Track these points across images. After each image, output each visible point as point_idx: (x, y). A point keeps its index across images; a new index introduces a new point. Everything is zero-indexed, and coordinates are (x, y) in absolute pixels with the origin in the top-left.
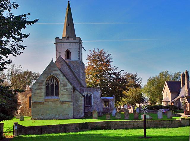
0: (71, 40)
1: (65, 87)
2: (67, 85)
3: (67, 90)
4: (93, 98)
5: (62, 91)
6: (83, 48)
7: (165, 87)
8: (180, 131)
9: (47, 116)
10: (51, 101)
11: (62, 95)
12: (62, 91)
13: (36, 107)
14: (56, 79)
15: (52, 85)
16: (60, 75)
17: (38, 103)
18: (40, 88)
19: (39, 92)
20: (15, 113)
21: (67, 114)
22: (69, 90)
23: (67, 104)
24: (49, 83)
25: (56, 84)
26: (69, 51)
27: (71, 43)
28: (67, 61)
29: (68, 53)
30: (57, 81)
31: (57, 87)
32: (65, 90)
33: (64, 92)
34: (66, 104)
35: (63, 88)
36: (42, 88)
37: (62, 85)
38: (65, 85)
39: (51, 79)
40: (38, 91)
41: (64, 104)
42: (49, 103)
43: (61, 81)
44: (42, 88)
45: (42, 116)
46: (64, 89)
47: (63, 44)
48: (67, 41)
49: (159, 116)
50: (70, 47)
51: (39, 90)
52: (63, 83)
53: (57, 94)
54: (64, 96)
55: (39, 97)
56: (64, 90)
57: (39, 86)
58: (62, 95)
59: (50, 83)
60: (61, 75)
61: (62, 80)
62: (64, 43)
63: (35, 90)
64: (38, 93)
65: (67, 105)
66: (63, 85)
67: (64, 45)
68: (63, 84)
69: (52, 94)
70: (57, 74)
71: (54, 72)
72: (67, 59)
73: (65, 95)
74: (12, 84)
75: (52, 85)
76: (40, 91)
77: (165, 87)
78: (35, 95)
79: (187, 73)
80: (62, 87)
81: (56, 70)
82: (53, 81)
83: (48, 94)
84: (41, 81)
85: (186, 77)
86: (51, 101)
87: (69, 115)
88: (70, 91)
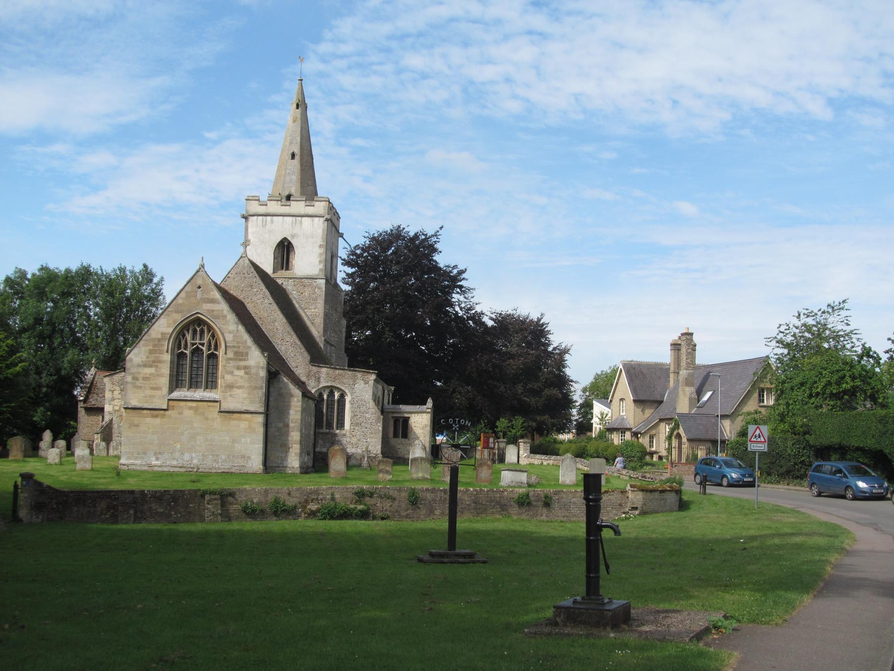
0: (298, 207)
1: (241, 360)
2: (247, 354)
3: (246, 373)
4: (348, 406)
5: (228, 371)
6: (341, 235)
7: (617, 383)
8: (752, 544)
9: (174, 459)
10: (191, 408)
11: (230, 387)
12: (232, 373)
13: (137, 426)
14: (210, 328)
15: (197, 351)
16: (226, 317)
17: (145, 412)
18: (154, 362)
19: (151, 374)
20: (35, 478)
21: (243, 457)
22: (253, 371)
23: (246, 420)
24: (186, 345)
25: (209, 350)
26: (290, 243)
27: (299, 218)
28: (281, 278)
29: (285, 250)
30: (213, 336)
31: (213, 357)
32: (241, 373)
33: (236, 378)
34: (240, 419)
35: (232, 363)
36: (160, 362)
37: (230, 354)
38: (241, 355)
39: (195, 331)
40: (148, 371)
41: (235, 419)
42: (181, 413)
43: (229, 337)
44: (160, 362)
45: (157, 459)
46: (238, 368)
47: (269, 218)
48: (285, 210)
49: (563, 476)
50: (295, 232)
51: (151, 366)
52: (233, 347)
53: (211, 384)
54: (237, 391)
55: (148, 392)
56: (237, 372)
57: (151, 352)
58: (230, 387)
59: (189, 344)
60: (231, 317)
61: (232, 335)
62: (275, 218)
63: (139, 366)
64: (145, 379)
65: (243, 425)
66: (236, 353)
67: (272, 222)
68: (235, 349)
69: (194, 384)
70: (215, 313)
71: (207, 306)
72: (282, 269)
73: (240, 387)
74: (744, 476)
75: (197, 351)
76: (152, 370)
77: (617, 383)
78: (138, 383)
79: (688, 335)
80: (231, 359)
81: (213, 301)
82: (201, 338)
83: (176, 382)
84: (160, 336)
85: (684, 350)
86: (191, 408)
87: (249, 458)
88: (257, 374)
